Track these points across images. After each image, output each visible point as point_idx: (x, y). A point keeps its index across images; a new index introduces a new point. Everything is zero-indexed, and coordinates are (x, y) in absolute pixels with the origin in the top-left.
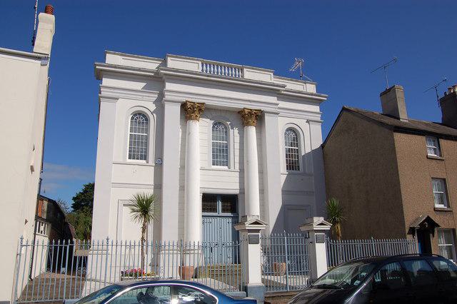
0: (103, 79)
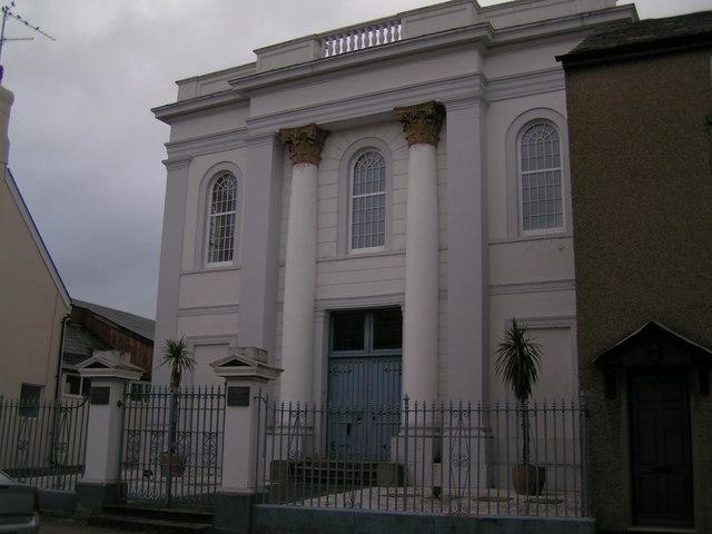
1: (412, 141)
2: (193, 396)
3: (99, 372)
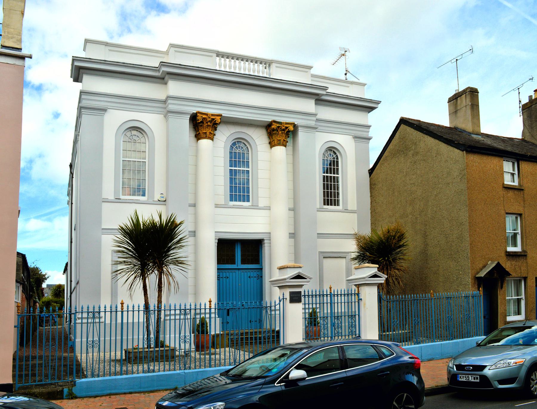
0: (402, 125)
1: (272, 145)
2: (323, 295)
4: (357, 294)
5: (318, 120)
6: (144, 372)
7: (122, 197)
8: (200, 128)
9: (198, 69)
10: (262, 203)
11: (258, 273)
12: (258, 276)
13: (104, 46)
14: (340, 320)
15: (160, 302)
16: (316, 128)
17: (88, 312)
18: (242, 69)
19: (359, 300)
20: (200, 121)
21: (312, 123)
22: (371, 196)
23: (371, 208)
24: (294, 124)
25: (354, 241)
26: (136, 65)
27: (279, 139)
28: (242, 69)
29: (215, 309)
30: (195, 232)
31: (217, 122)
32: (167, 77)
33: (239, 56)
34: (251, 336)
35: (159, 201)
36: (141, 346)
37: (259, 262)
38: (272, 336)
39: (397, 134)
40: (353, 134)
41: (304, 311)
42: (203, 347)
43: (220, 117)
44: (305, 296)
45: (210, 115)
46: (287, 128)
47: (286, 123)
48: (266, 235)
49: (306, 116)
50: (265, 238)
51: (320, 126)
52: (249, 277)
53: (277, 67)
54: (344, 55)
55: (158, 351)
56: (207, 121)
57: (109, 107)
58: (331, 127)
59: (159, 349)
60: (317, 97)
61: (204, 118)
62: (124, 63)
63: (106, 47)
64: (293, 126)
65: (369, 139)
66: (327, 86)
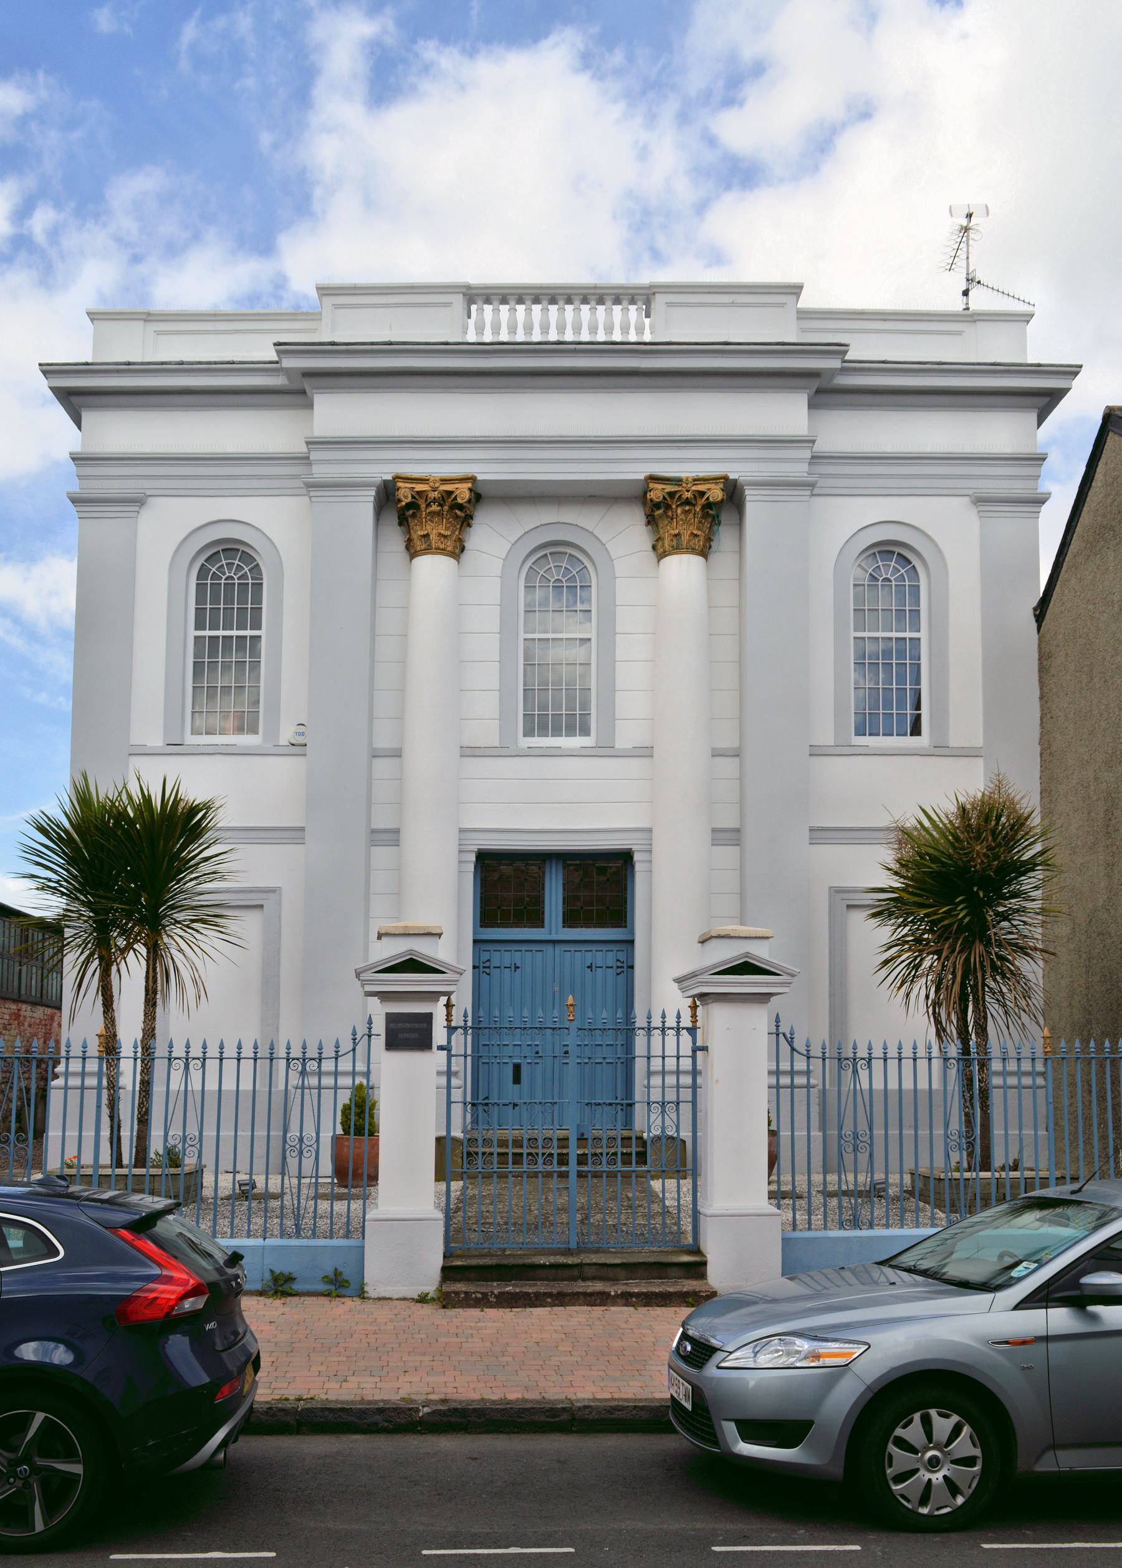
1: (660, 551)
3: (768, 984)
4: (687, 1029)
5: (816, 459)
6: (283, 1234)
7: (191, 739)
8: (412, 523)
9: (389, 348)
10: (627, 736)
11: (621, 956)
12: (619, 964)
13: (142, 322)
14: (674, 1116)
15: (149, 1033)
16: (812, 485)
17: (288, 1060)
18: (632, 331)
19: (695, 1049)
20: (404, 503)
21: (799, 470)
22: (1041, 698)
23: (1041, 739)
24: (726, 478)
25: (891, 852)
26: (215, 363)
27: (695, 532)
28: (632, 331)
29: (135, 1059)
30: (737, 831)
31: (460, 501)
32: (307, 384)
33: (539, 291)
34: (560, 1151)
35: (293, 745)
36: (87, 1159)
37: (626, 922)
38: (623, 1154)
39: (1098, 470)
40: (970, 492)
41: (699, 1080)
42: (357, 1176)
43: (470, 485)
44: (649, 1030)
45: (435, 481)
46: (702, 494)
47: (442, 480)
48: (640, 835)
49: (775, 448)
50: (634, 848)
51: (822, 475)
52: (517, 968)
53: (669, 304)
54: (966, 229)
55: (127, 1175)
56: (429, 500)
57: (149, 492)
58: (891, 476)
59: (148, 1171)
60: (815, 384)
61: (418, 492)
62: (182, 363)
63: (148, 324)
64: (721, 486)
65: (1042, 501)
66: (843, 342)
